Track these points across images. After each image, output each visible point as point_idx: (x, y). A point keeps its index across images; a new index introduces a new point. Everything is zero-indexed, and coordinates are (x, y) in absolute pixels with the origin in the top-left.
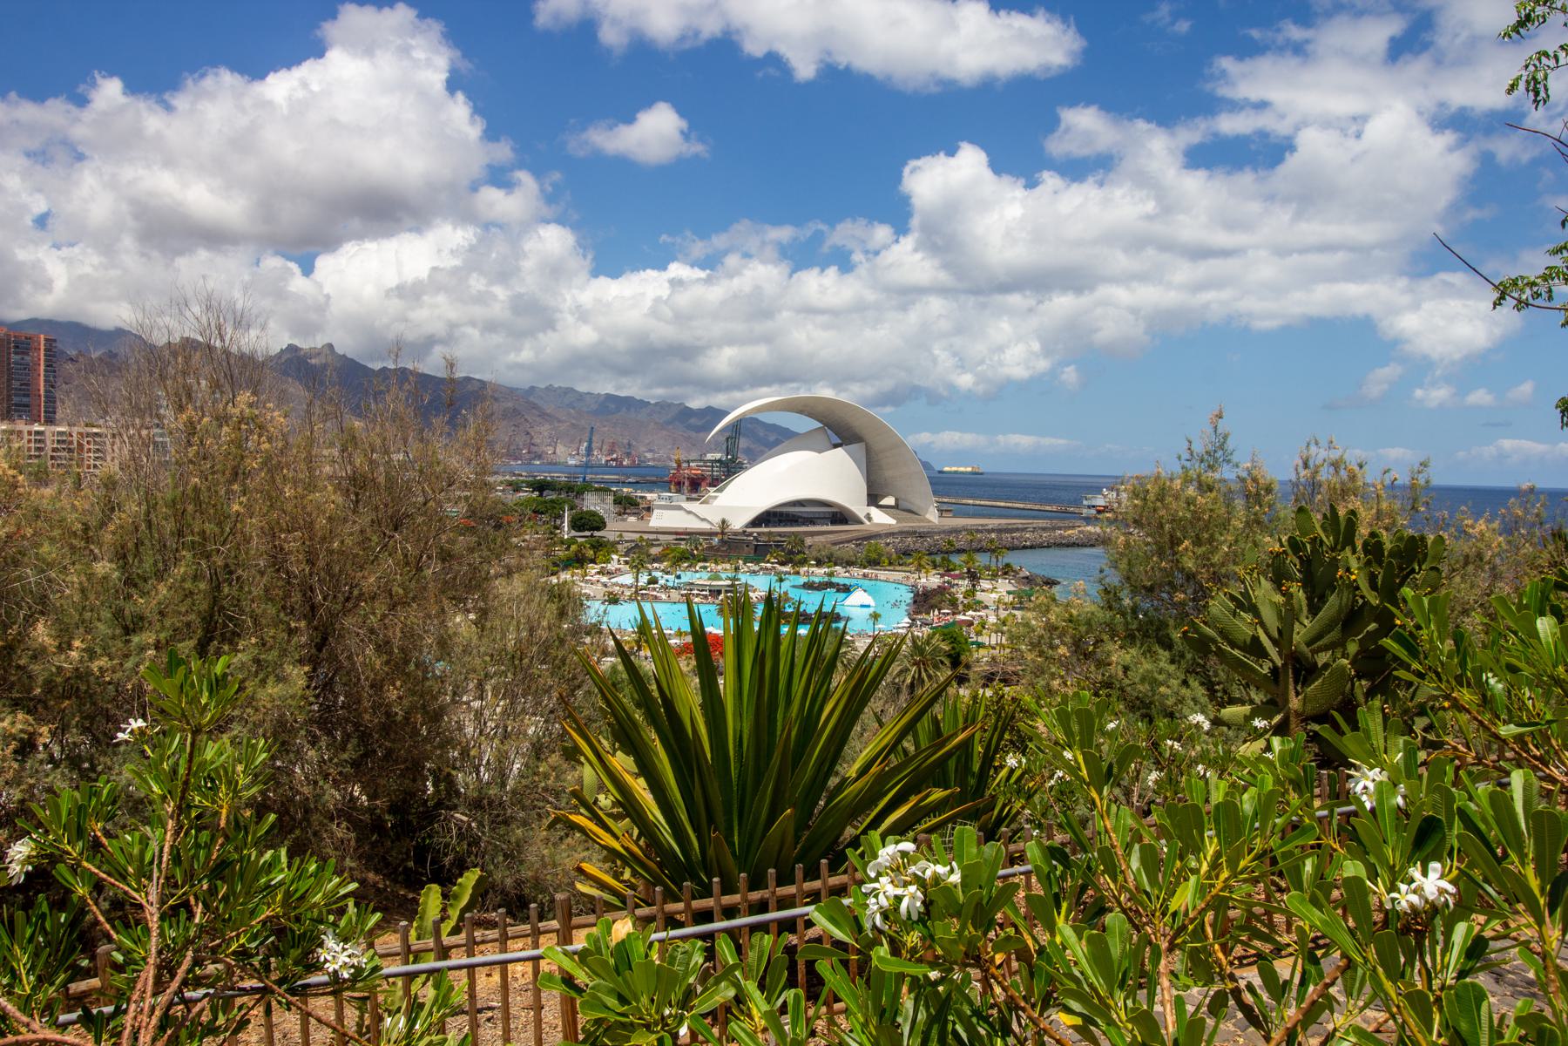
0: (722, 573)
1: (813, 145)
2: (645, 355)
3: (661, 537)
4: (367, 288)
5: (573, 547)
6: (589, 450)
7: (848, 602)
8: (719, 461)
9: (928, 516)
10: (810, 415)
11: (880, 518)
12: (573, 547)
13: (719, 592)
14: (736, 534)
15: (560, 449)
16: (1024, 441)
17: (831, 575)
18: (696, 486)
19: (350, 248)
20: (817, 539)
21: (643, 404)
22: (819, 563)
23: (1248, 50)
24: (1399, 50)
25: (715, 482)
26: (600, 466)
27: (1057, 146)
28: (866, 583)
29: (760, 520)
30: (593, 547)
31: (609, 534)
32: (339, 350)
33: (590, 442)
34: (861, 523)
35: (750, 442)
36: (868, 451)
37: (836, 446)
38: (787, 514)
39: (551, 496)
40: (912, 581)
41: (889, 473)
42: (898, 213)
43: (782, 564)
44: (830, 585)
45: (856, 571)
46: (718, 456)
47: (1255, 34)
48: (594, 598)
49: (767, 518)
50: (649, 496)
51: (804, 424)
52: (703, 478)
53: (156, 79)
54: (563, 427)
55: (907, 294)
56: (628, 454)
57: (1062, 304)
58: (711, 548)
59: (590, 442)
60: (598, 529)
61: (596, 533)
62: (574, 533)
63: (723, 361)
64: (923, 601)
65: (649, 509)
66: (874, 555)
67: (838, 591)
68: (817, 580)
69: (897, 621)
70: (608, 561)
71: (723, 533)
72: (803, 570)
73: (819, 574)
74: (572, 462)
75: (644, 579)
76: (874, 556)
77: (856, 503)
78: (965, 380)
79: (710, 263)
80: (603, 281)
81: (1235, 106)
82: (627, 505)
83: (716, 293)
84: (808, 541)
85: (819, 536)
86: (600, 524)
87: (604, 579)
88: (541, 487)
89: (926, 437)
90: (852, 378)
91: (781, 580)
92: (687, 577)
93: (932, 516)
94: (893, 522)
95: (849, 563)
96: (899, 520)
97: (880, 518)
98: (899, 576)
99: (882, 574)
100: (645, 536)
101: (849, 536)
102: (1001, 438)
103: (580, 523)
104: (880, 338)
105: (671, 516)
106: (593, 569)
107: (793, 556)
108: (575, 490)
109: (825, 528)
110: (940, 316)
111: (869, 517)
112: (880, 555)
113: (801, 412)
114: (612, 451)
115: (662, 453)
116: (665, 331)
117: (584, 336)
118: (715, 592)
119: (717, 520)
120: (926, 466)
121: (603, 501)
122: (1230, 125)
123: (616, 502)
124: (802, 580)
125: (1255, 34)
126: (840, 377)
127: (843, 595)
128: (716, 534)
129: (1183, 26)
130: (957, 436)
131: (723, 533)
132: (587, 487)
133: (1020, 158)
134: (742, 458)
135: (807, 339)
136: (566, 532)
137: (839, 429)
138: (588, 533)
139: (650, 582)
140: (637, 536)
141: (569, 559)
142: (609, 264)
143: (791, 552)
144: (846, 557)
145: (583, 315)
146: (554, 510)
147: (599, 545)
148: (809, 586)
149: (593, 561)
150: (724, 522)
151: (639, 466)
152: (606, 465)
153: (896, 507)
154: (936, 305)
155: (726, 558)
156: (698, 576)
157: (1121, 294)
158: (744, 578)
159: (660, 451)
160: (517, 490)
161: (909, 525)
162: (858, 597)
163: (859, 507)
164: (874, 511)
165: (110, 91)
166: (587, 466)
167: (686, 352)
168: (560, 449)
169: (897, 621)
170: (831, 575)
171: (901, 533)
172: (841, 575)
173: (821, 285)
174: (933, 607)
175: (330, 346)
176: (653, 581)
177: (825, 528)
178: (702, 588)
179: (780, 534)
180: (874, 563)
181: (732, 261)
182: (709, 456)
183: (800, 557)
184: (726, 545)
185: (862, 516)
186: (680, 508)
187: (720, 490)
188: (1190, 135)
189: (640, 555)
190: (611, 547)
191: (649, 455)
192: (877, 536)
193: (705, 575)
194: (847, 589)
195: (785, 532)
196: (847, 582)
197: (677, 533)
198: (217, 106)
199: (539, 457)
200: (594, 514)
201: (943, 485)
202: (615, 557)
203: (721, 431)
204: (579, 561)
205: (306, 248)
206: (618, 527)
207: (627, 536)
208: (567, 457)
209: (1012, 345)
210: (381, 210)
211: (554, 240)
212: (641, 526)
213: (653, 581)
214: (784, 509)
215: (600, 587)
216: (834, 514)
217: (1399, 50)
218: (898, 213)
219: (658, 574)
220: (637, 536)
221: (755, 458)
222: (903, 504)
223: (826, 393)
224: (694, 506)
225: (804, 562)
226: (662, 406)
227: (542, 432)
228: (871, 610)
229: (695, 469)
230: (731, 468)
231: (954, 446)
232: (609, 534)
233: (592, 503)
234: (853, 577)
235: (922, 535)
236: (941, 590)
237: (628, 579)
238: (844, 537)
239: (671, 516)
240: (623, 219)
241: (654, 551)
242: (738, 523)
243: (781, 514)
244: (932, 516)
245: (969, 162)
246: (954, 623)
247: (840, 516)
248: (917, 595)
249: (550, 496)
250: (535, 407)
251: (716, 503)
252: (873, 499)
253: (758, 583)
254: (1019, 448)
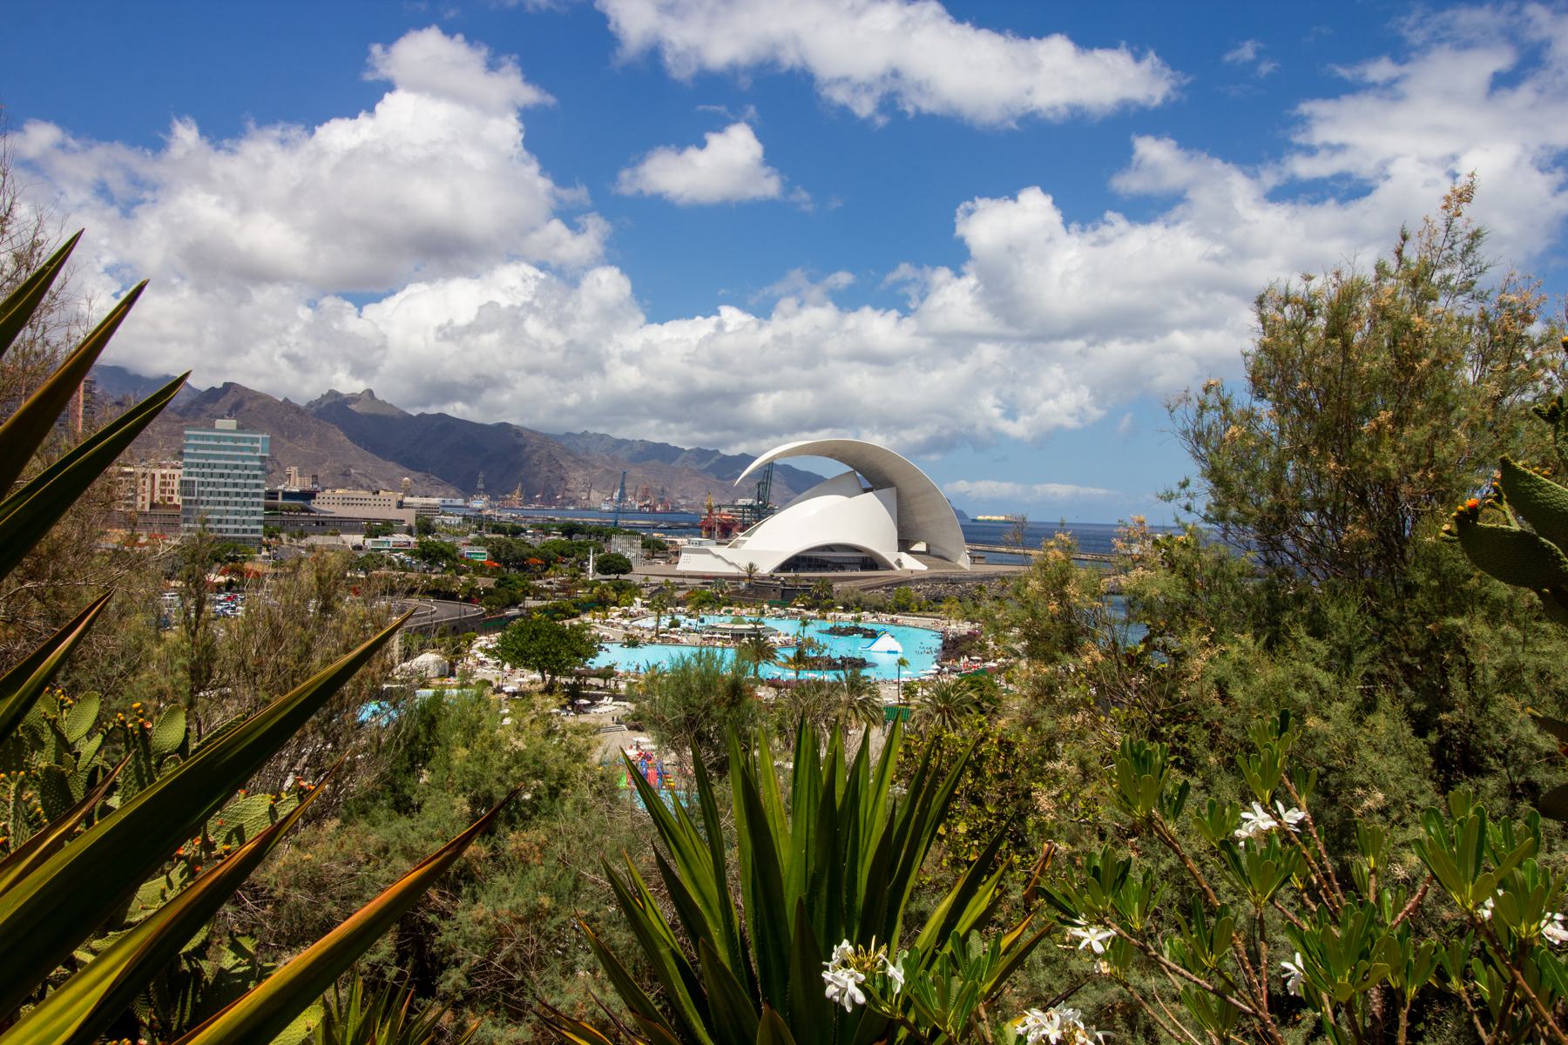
0: (745, 618)
1: (871, 187)
2: (692, 403)
3: (687, 581)
4: (423, 335)
5: (596, 590)
6: (623, 496)
7: (873, 648)
8: (750, 506)
9: (960, 563)
10: (842, 459)
11: (911, 564)
12: (596, 590)
13: (742, 636)
14: (763, 578)
15: (594, 495)
16: (1060, 490)
17: (858, 620)
18: (726, 532)
19: (412, 289)
20: (846, 584)
21: (677, 451)
22: (847, 609)
23: (1337, 90)
24: (1503, 82)
25: (745, 527)
26: (634, 512)
27: (1128, 184)
28: (893, 628)
29: (785, 566)
30: (616, 589)
31: (635, 577)
32: (379, 396)
33: (623, 488)
34: (891, 568)
35: (777, 487)
36: (899, 495)
37: (866, 491)
38: (817, 560)
39: (579, 537)
40: (941, 628)
41: (920, 519)
42: (957, 256)
43: (808, 608)
44: (856, 630)
45: (884, 617)
46: (749, 501)
47: (1344, 72)
48: (613, 641)
49: (796, 563)
50: (679, 541)
51: (837, 468)
52: (734, 524)
53: (223, 130)
54: (598, 473)
55: (957, 342)
56: (662, 501)
57: (1117, 351)
58: (738, 592)
59: (623, 488)
60: (624, 572)
61: (622, 577)
62: (599, 576)
63: (764, 406)
64: (952, 648)
65: (677, 554)
66: (902, 600)
67: (865, 636)
68: (844, 625)
69: (924, 668)
70: (630, 604)
71: (750, 577)
72: (829, 615)
73: (847, 619)
74: (606, 508)
75: (666, 622)
76: (902, 601)
77: (886, 548)
78: (1017, 429)
79: (763, 312)
80: (655, 328)
81: (1310, 151)
82: (655, 549)
83: (766, 335)
84: (837, 586)
85: (846, 582)
86: (626, 567)
87: (626, 622)
88: (569, 530)
89: (962, 486)
90: (901, 425)
91: (805, 624)
92: (711, 620)
93: (964, 563)
94: (925, 568)
95: (878, 609)
96: (930, 567)
97: (911, 564)
98: (929, 622)
99: (910, 620)
100: (672, 580)
101: (879, 581)
102: (1038, 488)
103: (605, 566)
104: (935, 384)
105: (700, 560)
106: (615, 612)
107: (821, 601)
108: (603, 533)
109: (854, 574)
110: (995, 363)
111: (899, 563)
112: (909, 600)
113: (831, 456)
114: (645, 498)
115: (695, 500)
116: (705, 378)
117: (627, 378)
118: (737, 636)
119: (744, 564)
120: (960, 514)
121: (632, 545)
122: (1304, 168)
123: (644, 546)
124: (828, 625)
125: (1344, 72)
126: (887, 423)
127: (869, 641)
128: (743, 578)
129: (1266, 68)
130: (993, 485)
131: (750, 577)
132: (617, 530)
133: (1083, 207)
134: (773, 504)
135: (861, 384)
136: (591, 574)
137: (870, 474)
138: (613, 576)
139: (671, 625)
140: (663, 580)
141: (591, 601)
142: (659, 314)
143: (818, 597)
144: (875, 602)
145: (630, 358)
146: (583, 548)
147: (621, 588)
148: (833, 631)
149: (616, 604)
150: (751, 566)
151: (672, 512)
152: (640, 511)
153: (928, 552)
154: (989, 353)
155: (750, 603)
156: (721, 620)
157: (1180, 338)
158: (769, 622)
159: (693, 497)
160: (548, 534)
161: (937, 572)
162: (885, 642)
163: (890, 553)
164: (904, 556)
165: (186, 135)
166: (618, 512)
167: (735, 397)
168: (594, 495)
169: (924, 668)
170: (858, 620)
171: (932, 579)
172: (869, 620)
173: (879, 328)
174: (962, 654)
175: (370, 392)
176: (675, 624)
177: (854, 574)
178: (724, 631)
179: (808, 579)
180: (903, 609)
181: (787, 304)
182: (740, 502)
183: (827, 602)
184: (753, 590)
185: (892, 562)
186: (708, 552)
187: (749, 535)
188: (1270, 179)
189: (662, 598)
190: (635, 590)
191: (683, 502)
192: (907, 582)
193: (729, 618)
194: (873, 635)
195: (814, 577)
196: (877, 628)
197: (704, 577)
198: (267, 160)
199: (573, 502)
200: (620, 557)
201: (978, 535)
202: (638, 600)
203: (749, 476)
204: (601, 604)
205: (365, 292)
206: (644, 571)
207: (654, 580)
208: (600, 503)
209: (1060, 395)
210: (443, 251)
211: (609, 283)
212: (669, 570)
213: (675, 624)
214: (813, 554)
215: (620, 630)
216: (864, 560)
217: (1503, 82)
218: (957, 256)
219: (680, 617)
220: (663, 580)
221: (786, 503)
222: (933, 550)
223: (877, 440)
224: (722, 551)
225: (831, 607)
226: (701, 454)
227: (577, 478)
228: (899, 656)
229: (725, 514)
230: (761, 512)
231: (989, 494)
232: (635, 577)
233: (629, 549)
234: (880, 622)
235: (953, 582)
236: (971, 636)
237: (650, 622)
238: (873, 582)
239: (700, 560)
240: (681, 259)
241: (679, 594)
242: (765, 568)
243: (810, 559)
244: (964, 563)
245: (1033, 209)
246: (984, 671)
247: (870, 562)
248: (946, 641)
249: (579, 538)
250: (570, 453)
251: (744, 547)
252: (904, 545)
253: (783, 628)
254: (1056, 496)
